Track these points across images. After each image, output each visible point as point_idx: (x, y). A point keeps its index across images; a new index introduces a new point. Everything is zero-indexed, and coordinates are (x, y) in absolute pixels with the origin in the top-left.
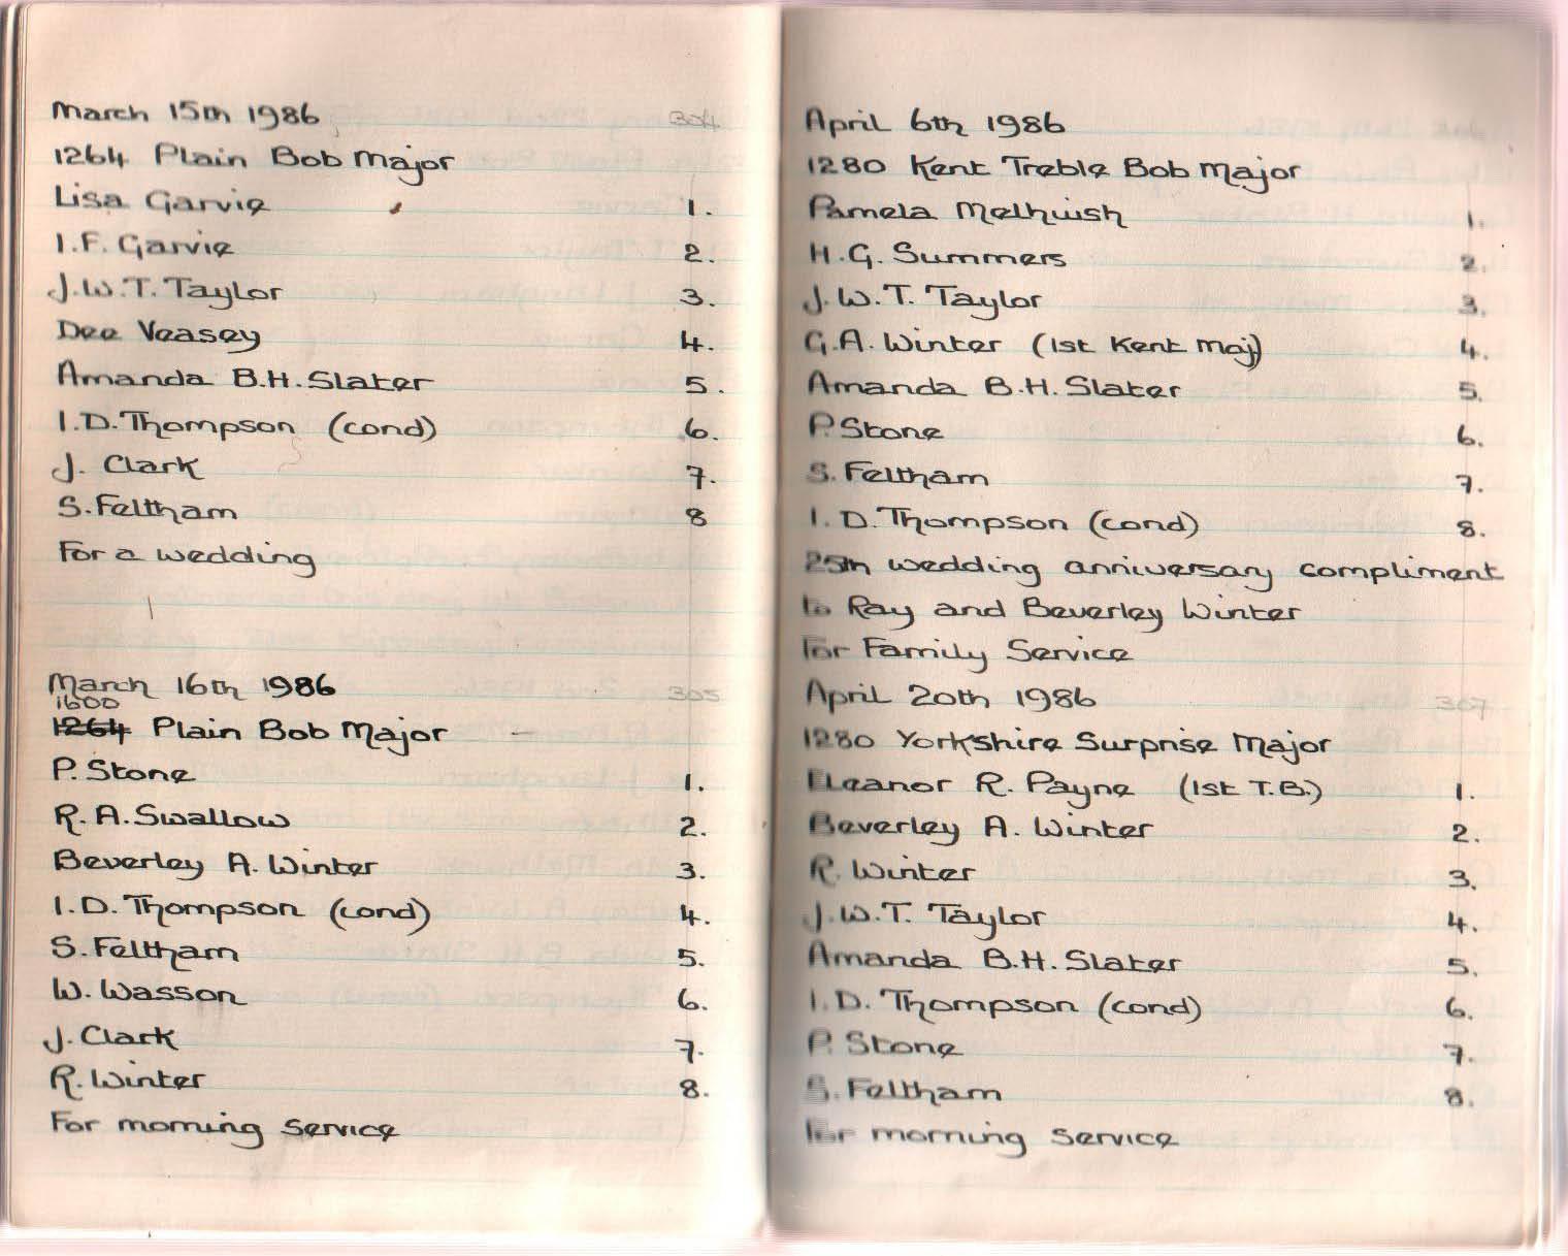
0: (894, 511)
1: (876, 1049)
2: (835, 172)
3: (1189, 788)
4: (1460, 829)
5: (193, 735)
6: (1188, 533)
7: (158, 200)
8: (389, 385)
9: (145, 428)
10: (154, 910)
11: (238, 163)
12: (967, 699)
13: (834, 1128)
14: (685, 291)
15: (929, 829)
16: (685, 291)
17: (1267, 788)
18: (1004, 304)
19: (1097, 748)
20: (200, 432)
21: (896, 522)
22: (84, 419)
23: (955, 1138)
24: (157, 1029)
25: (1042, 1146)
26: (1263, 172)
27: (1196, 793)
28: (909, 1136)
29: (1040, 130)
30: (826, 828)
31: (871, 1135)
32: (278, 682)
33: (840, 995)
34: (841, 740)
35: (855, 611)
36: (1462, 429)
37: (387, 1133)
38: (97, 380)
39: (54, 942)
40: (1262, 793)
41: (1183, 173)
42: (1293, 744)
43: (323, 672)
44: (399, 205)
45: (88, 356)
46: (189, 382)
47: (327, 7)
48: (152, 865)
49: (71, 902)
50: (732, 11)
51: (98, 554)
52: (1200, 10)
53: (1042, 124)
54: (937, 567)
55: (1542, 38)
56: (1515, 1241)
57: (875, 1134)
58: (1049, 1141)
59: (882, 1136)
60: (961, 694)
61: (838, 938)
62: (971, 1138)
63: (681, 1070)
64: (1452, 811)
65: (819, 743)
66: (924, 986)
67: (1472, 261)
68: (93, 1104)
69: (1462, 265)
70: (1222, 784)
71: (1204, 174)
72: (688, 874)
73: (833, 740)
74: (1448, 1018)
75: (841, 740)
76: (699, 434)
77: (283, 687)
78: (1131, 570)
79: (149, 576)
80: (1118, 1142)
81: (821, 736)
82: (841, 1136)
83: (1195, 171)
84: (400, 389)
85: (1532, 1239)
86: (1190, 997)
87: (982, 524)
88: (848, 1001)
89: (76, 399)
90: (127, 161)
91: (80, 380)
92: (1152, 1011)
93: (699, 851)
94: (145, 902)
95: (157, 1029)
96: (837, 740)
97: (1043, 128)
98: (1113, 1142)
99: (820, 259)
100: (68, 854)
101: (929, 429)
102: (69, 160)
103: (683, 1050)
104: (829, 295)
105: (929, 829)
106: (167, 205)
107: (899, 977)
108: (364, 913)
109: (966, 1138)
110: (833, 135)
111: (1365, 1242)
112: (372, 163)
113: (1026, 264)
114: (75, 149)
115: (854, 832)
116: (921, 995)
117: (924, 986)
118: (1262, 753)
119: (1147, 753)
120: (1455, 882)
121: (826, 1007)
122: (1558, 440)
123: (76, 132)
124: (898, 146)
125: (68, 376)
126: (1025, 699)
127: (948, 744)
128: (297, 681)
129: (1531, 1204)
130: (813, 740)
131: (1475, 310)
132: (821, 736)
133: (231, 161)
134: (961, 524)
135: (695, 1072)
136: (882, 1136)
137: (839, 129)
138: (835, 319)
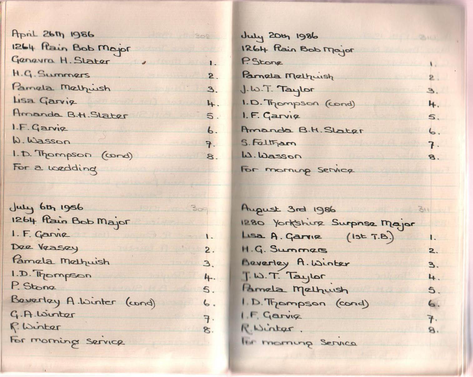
0: (269, 299)
1: (278, 330)
2: (250, 224)
3: (351, 236)
4: (207, 249)
5: (52, 222)
6: (353, 106)
7: (15, 59)
8: (115, 117)
9: (43, 155)
10: (42, 275)
11: (64, 50)
12: (49, 207)
13: (250, 340)
14: (205, 261)
15: (67, 248)
16: (205, 261)
17: (377, 237)
18: (301, 91)
19: (338, 224)
20: (251, 133)
21: (40, 155)
22: (22, 153)
23: (290, 343)
24: (290, 220)
25: (318, 347)
26: (343, 50)
27: (354, 238)
28: (274, 343)
29: (86, 36)
30: (247, 263)
31: (262, 343)
32: (67, 207)
33: (253, 300)
34: (253, 223)
35: (244, 329)
36: (209, 128)
37: (120, 343)
38: (26, 114)
39: (24, 285)
40: (375, 239)
41: (92, 49)
42: (117, 222)
43: (41, 202)
44: (145, 62)
45: (22, 107)
46: (55, 115)
47: (97, 2)
48: (42, 301)
49: (17, 273)
50: (217, 3)
51: (254, 170)
52: (358, 2)
53: (87, 34)
54: (63, 169)
55: (462, 10)
56: (456, 374)
57: (263, 342)
58: (320, 344)
59: (266, 343)
60: (47, 206)
61: (254, 283)
62: (295, 343)
63: (204, 323)
64: (429, 244)
65: (246, 224)
66: (277, 297)
67: (212, 75)
68: (21, 333)
69: (429, 78)
70: (361, 235)
71: (325, 50)
72: (208, 264)
73: (250, 223)
74: (429, 307)
75: (253, 223)
76: (433, 133)
77: (321, 210)
78: (294, 171)
79: (46, 173)
80: (106, 343)
81: (246, 222)
82: (252, 342)
83: (322, 50)
84: (118, 118)
85: (460, 374)
86: (365, 300)
87: (293, 104)
88: (255, 302)
89: (18, 120)
90: (35, 49)
91: (21, 115)
92: (141, 304)
93: (214, 110)
94: (40, 272)
95: (290, 220)
96: (252, 223)
97: (88, 35)
98: (104, 343)
99: (245, 250)
100: (76, 219)
101: (354, 130)
102: (17, 221)
103: (429, 318)
104: (248, 88)
105: (67, 248)
106: (18, 60)
107: (269, 295)
108: (317, 277)
109: (293, 343)
110: (21, 38)
111: (381, 375)
112: (104, 49)
113: (267, 78)
114: (249, 46)
115: (315, 252)
116: (275, 101)
117: (277, 297)
118: (391, 226)
119: (353, 226)
120: (430, 266)
121: (248, 304)
122: (468, 131)
123: (17, 40)
124: (269, 43)
125: (17, 113)
126: (316, 210)
127: (289, 224)
128: (326, 208)
129: (460, 363)
130: (244, 223)
131: (434, 92)
132: (246, 222)
133: (63, 49)
134: (59, 155)
135: (434, 325)
136: (266, 343)
137: (23, 36)
138: (249, 96)
